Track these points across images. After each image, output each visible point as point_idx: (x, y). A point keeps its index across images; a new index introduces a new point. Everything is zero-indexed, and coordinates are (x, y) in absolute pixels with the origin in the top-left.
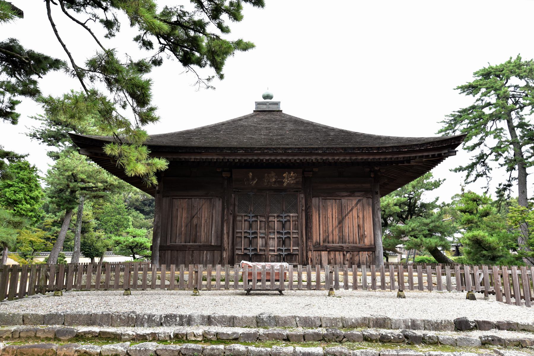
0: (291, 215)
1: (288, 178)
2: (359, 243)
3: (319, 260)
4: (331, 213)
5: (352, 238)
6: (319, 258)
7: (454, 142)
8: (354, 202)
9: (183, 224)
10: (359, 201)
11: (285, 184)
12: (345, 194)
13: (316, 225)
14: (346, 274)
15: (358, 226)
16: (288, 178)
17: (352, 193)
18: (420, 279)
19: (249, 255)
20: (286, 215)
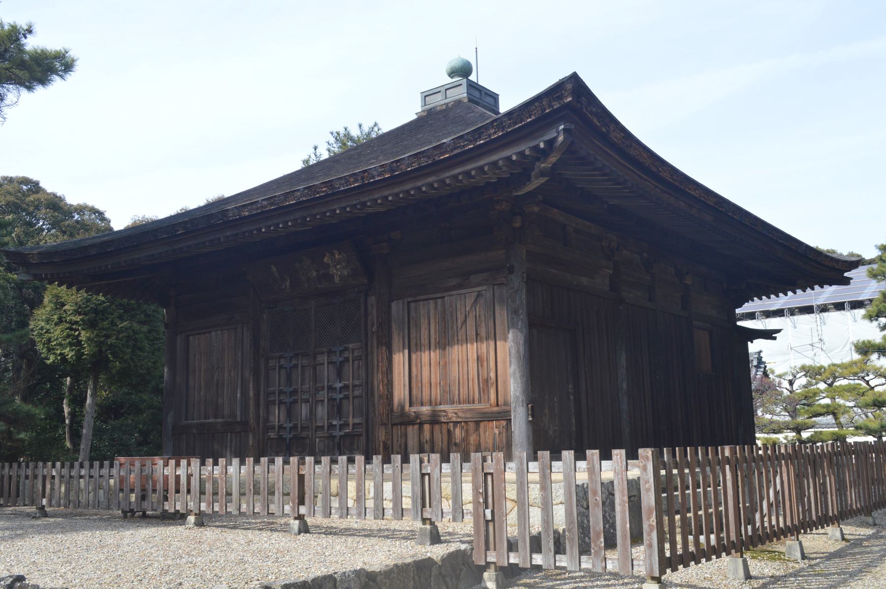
0: (351, 346)
1: (335, 266)
2: (480, 402)
3: (403, 446)
4: (427, 333)
5: (428, 392)
6: (403, 440)
7: (550, 106)
8: (469, 301)
9: (203, 384)
10: (479, 295)
11: (337, 279)
12: (454, 282)
13: (399, 365)
14: (522, 473)
15: (479, 359)
16: (335, 266)
17: (464, 280)
18: (379, 496)
19: (285, 439)
20: (341, 348)
